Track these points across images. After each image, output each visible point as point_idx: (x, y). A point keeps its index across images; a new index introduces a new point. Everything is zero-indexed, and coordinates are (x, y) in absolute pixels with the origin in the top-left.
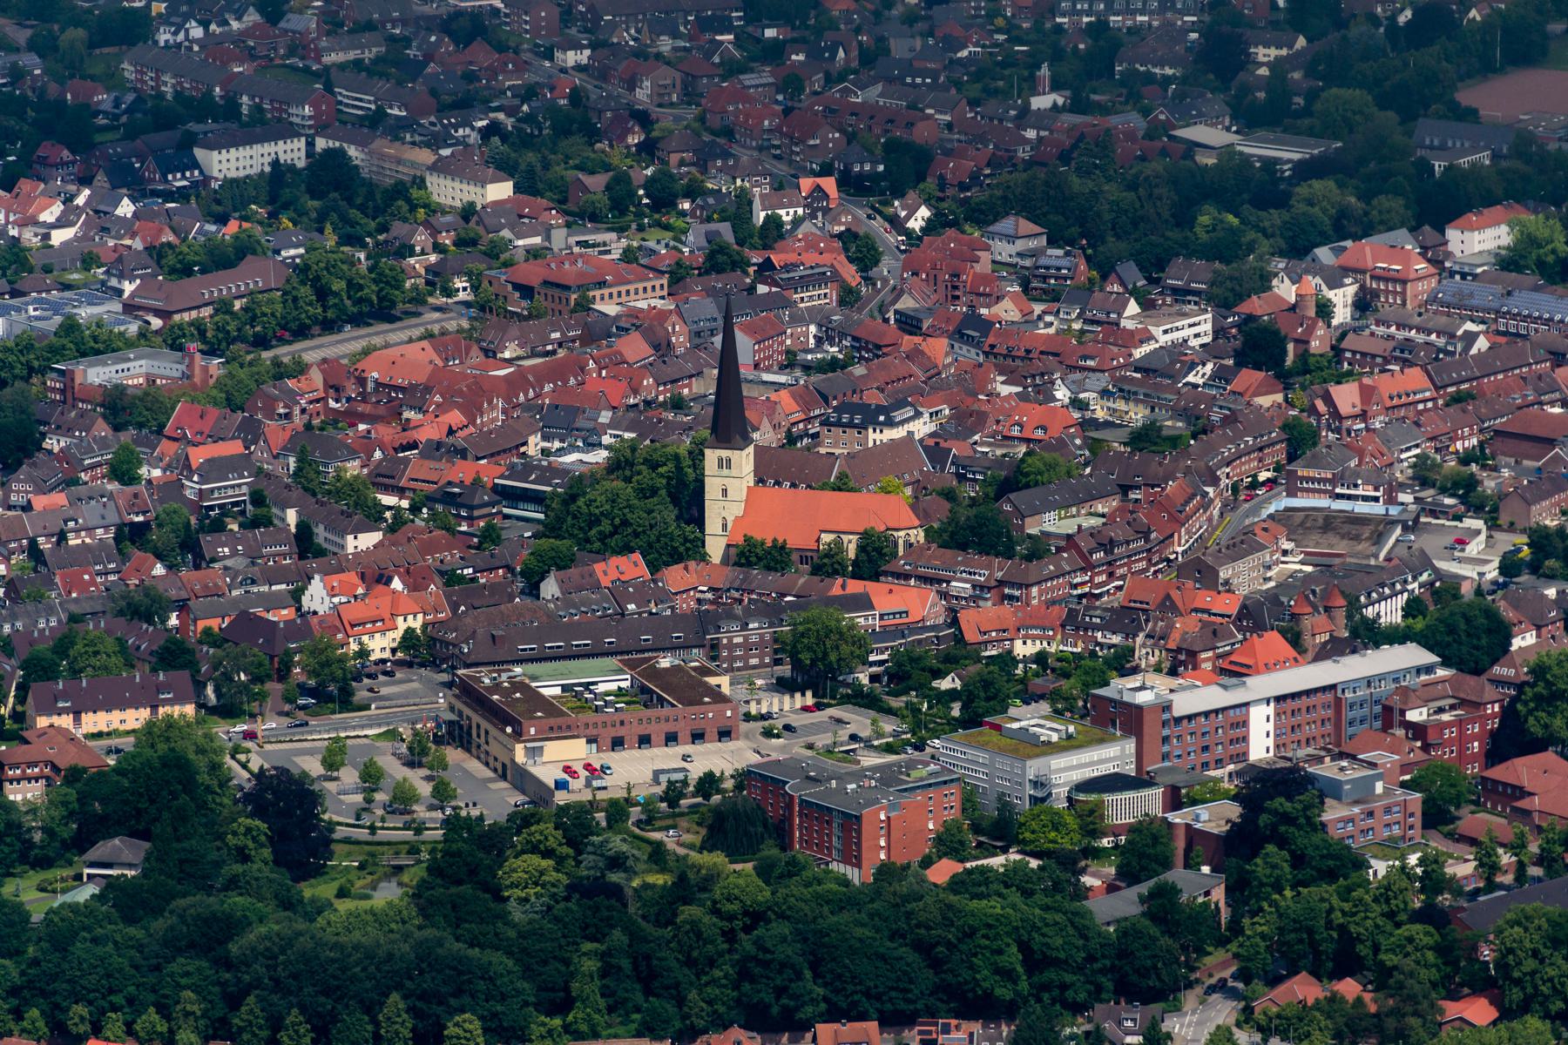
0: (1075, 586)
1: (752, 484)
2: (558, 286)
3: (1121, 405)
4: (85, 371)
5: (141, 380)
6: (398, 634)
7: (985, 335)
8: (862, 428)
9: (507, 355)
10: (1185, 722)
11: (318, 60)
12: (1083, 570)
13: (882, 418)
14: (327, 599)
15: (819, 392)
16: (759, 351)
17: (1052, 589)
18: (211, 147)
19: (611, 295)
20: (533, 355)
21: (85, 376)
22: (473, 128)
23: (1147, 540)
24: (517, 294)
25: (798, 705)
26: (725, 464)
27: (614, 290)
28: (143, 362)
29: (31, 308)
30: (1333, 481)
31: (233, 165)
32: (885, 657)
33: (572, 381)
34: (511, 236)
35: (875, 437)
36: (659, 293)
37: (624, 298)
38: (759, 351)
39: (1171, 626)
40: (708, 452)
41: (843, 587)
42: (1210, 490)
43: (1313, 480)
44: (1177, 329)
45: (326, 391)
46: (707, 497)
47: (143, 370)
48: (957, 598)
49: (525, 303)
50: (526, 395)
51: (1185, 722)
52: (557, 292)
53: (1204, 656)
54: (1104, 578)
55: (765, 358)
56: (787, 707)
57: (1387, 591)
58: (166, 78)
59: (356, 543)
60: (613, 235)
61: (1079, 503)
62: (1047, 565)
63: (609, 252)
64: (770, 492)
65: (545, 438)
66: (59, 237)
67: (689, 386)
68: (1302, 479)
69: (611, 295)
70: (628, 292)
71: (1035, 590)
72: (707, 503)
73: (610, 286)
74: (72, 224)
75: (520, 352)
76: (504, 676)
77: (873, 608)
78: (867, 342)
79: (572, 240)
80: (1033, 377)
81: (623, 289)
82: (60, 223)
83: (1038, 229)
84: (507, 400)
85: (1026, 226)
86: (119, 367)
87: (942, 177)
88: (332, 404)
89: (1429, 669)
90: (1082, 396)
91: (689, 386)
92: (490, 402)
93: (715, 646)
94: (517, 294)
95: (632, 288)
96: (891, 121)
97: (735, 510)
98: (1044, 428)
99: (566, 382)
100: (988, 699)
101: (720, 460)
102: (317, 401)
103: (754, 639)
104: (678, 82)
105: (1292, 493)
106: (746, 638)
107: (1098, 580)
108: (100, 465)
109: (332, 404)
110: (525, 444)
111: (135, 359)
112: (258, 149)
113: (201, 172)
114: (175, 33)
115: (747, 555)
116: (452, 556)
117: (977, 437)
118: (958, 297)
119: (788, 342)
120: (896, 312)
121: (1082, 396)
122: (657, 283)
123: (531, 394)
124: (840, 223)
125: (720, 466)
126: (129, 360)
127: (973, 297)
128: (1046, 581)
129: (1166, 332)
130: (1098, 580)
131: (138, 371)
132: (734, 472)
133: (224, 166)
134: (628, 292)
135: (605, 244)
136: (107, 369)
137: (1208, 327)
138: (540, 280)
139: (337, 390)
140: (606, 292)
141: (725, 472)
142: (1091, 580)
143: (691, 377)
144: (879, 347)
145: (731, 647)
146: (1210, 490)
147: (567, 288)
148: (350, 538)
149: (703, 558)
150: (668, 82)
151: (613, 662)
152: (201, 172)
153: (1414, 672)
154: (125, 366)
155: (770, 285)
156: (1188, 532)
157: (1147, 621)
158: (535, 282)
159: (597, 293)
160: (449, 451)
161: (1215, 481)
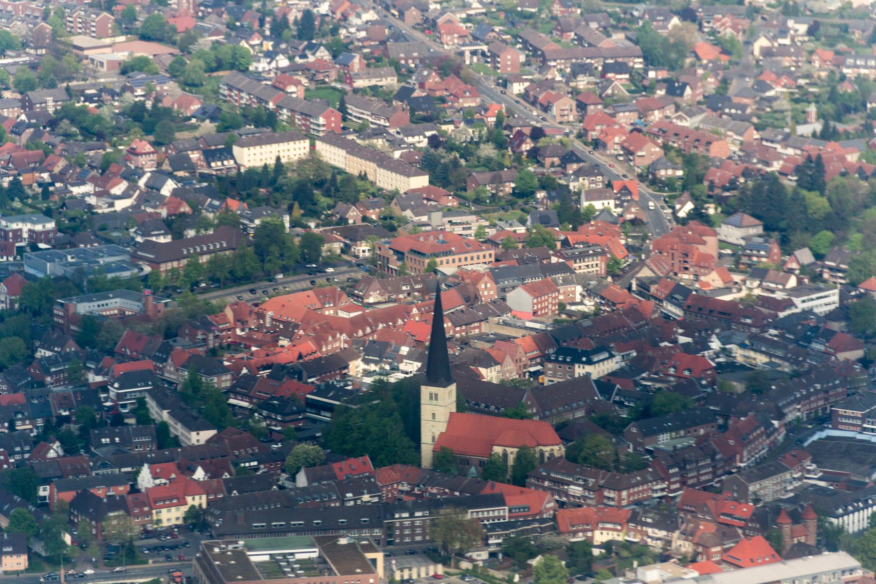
0: (656, 491)
1: (454, 410)
2: (419, 253)
3: (752, 354)
4: (76, 305)
5: (116, 312)
6: (185, 508)
7: (685, 299)
8: (572, 363)
9: (371, 300)
10: (848, 573)
11: (351, 84)
12: (663, 480)
13: (584, 359)
14: (152, 480)
15: (554, 337)
16: (537, 304)
17: (638, 493)
18: (242, 145)
19: (454, 261)
20: (389, 301)
21: (76, 309)
22: (425, 137)
23: (713, 459)
24: (395, 257)
25: (431, 573)
26: (434, 397)
27: (456, 257)
28: (117, 300)
29: (69, 257)
30: (863, 419)
31: (258, 157)
32: (500, 541)
33: (400, 322)
34: (412, 215)
35: (580, 370)
36: (488, 259)
37: (463, 262)
38: (537, 304)
39: (697, 527)
40: (423, 388)
41: (492, 487)
42: (776, 423)
43: (849, 417)
44: (812, 300)
45: (235, 323)
46: (423, 418)
47: (118, 305)
48: (574, 496)
49: (399, 263)
50: (364, 331)
51: (848, 573)
52: (417, 258)
53: (714, 550)
54: (678, 486)
55: (541, 309)
56: (423, 575)
57: (861, 505)
58: (243, 95)
59: (198, 438)
60: (474, 218)
61: (684, 426)
62: (635, 477)
63: (470, 228)
64: (470, 417)
65: (366, 362)
66: (120, 205)
67: (479, 327)
68: (842, 416)
69: (454, 261)
70: (466, 259)
71: (624, 494)
72: (423, 422)
73: (454, 254)
74: (130, 196)
75: (381, 299)
76: (230, 547)
77: (504, 504)
78: (608, 300)
79: (446, 220)
80: (700, 331)
81: (463, 256)
82: (125, 196)
83: (757, 222)
84: (350, 335)
85: (748, 219)
86: (100, 303)
87: (712, 182)
88: (239, 332)
89: (852, 571)
90: (728, 346)
91: (479, 327)
92: (334, 337)
93: (390, 528)
94: (395, 257)
95: (469, 256)
96: (698, 140)
97: (442, 427)
98: (690, 370)
99: (395, 322)
100: (550, 577)
101: (431, 394)
102: (229, 330)
103: (418, 523)
104: (574, 107)
105: (835, 428)
106: (413, 522)
107: (673, 487)
108: (62, 371)
109: (239, 332)
110: (346, 367)
111: (114, 297)
112: (267, 148)
113: (236, 162)
114: (269, 63)
115: (445, 459)
116: (246, 452)
117: (644, 375)
118: (686, 269)
119: (561, 297)
120: (638, 279)
121: (728, 346)
122: (487, 253)
123: (368, 330)
124: (631, 213)
125: (431, 398)
126: (109, 298)
127: (697, 269)
128: (633, 487)
129: (804, 301)
130: (673, 487)
131: (114, 305)
132: (440, 402)
133: (252, 158)
134: (466, 259)
135: (467, 223)
136: (91, 304)
137: (836, 298)
138: (408, 248)
139: (243, 323)
140: (450, 258)
141: (434, 402)
142: (668, 488)
143: (481, 321)
144: (614, 304)
145: (402, 528)
146: (776, 423)
147: (423, 255)
148: (194, 434)
149: (417, 461)
150: (567, 107)
151: (310, 537)
152: (236, 162)
153: (840, 573)
154: (104, 302)
155: (559, 257)
156: (749, 452)
157: (682, 522)
158: (405, 249)
159: (444, 259)
160: (289, 372)
161: (780, 416)
